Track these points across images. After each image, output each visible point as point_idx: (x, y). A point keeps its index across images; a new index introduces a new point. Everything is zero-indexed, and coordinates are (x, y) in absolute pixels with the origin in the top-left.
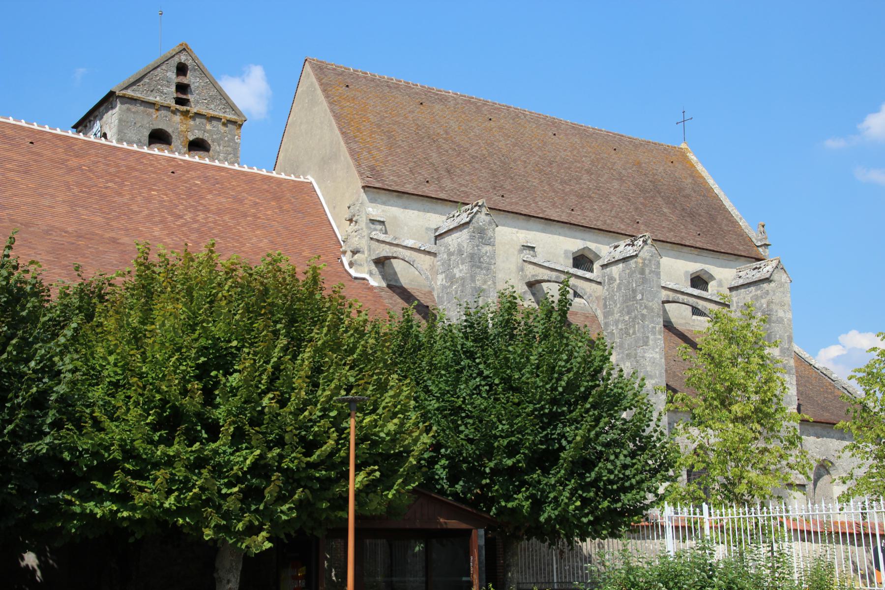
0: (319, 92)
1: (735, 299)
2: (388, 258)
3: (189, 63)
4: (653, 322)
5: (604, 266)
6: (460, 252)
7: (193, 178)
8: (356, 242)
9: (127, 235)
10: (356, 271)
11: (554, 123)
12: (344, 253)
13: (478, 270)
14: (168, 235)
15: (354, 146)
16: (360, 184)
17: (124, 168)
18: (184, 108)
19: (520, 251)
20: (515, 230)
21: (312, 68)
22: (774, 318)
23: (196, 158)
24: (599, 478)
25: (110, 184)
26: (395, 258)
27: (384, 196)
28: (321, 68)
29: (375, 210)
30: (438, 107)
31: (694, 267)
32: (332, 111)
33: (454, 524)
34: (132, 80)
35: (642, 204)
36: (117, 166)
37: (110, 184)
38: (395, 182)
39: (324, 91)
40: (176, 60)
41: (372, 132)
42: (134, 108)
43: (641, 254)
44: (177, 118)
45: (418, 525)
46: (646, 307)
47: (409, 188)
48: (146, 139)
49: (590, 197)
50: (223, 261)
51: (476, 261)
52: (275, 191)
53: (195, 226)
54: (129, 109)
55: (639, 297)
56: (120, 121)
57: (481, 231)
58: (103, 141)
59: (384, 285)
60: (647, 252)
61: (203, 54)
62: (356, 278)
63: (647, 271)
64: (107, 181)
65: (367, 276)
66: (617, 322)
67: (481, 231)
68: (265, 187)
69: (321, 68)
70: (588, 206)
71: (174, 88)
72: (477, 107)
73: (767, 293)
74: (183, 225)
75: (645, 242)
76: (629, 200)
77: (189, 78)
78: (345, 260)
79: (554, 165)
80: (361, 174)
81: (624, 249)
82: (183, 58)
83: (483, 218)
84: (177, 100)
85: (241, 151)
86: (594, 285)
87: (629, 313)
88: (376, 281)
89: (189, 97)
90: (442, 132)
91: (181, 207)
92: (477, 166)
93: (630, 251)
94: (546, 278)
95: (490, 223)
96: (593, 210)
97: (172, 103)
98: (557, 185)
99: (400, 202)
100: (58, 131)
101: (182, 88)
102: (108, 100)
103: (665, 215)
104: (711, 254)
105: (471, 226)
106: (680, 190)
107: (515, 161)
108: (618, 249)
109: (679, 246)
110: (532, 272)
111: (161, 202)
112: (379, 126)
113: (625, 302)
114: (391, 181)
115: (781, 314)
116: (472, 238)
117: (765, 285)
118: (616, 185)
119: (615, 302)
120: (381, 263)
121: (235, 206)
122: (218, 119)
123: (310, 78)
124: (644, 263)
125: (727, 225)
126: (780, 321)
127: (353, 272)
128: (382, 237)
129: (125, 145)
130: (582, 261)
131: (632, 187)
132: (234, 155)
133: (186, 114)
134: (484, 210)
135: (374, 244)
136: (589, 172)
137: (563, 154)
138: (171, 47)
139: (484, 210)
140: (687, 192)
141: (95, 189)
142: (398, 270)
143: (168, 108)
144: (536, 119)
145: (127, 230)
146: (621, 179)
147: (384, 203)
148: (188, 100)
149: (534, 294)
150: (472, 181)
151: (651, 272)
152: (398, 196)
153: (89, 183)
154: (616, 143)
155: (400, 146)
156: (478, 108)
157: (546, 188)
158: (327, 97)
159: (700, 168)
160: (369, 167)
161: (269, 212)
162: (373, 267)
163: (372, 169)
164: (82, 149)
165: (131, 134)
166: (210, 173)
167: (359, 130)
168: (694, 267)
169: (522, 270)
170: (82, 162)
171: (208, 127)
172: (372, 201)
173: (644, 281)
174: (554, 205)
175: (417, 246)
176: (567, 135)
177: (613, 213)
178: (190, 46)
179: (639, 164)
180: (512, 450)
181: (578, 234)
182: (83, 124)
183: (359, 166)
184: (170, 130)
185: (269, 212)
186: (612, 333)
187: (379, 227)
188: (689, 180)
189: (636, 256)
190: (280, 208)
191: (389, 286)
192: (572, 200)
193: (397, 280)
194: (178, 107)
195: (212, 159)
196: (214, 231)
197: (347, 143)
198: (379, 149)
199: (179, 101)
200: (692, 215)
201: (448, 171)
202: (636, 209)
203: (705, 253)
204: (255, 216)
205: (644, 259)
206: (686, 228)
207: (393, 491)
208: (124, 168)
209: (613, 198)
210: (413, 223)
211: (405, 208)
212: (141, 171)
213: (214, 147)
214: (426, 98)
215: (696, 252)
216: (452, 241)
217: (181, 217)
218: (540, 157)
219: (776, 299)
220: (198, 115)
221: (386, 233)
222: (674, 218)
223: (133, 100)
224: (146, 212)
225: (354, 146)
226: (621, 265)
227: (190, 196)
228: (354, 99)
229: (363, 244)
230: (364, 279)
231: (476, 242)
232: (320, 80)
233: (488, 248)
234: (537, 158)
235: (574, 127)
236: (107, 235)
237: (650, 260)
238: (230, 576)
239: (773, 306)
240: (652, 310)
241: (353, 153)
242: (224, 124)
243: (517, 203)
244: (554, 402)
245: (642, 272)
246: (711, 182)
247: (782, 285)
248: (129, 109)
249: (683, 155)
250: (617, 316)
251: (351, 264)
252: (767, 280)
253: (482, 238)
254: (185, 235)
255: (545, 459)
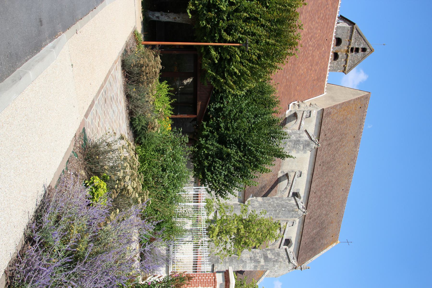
0: (358, 96)
1: (282, 250)
2: (288, 178)
3: (367, 53)
4: (274, 214)
5: (286, 249)
6: (300, 137)
7: (325, 47)
8: (302, 105)
9: (304, 18)
10: (292, 106)
11: (347, 190)
12: (298, 102)
13: (293, 143)
14: (304, 34)
15: (338, 107)
16: (324, 108)
17: (328, 21)
18: (350, 51)
19: (299, 171)
20: (307, 169)
21: (367, 95)
22: (275, 263)
23: (331, 57)
24: (215, 162)
25: (322, 15)
26: (288, 180)
27: (320, 117)
28: (367, 98)
29: (314, 114)
30: (353, 143)
31: (293, 240)
32: (351, 100)
33: (199, 108)
34: (359, 31)
35: (317, 222)
36: (329, 19)
37: (322, 15)
38: (325, 122)
39: (359, 98)
40: (368, 48)
41: (344, 115)
42: (349, 32)
43: (299, 210)
44: (346, 48)
45: (198, 93)
46: (279, 212)
47: (323, 127)
48: (338, 36)
49: (320, 201)
50: (298, 31)
51: (297, 142)
52: (321, 79)
53: (307, 45)
54: (348, 30)
55: (283, 209)
56: (344, 27)
57: (308, 145)
58: (336, 23)
59: (287, 116)
60: (300, 213)
61: (370, 58)
62: (289, 106)
63: (293, 213)
64: (323, 14)
65: (290, 109)
66: (273, 202)
67: (308, 145)
68: (322, 75)
69: (367, 98)
70: (316, 200)
71: (357, 47)
72: (353, 159)
73: (285, 261)
74: (308, 41)
75: (304, 212)
76: (318, 217)
77: (361, 53)
78: (296, 102)
79: (332, 188)
80: (328, 108)
81: (301, 205)
82: (368, 50)
83: (313, 145)
84: (352, 49)
85: (334, 73)
86: (287, 195)
87: (277, 206)
88: (288, 113)
89: (354, 53)
90: (344, 144)
91: (314, 41)
92: (331, 156)
93: (301, 207)
94: (290, 179)
95: (312, 148)
96: (315, 201)
97: (351, 46)
98: (324, 188)
99: (318, 123)
100: (338, 10)
101: (357, 50)
102: (352, 23)
103: (313, 230)
104: (298, 247)
105: (310, 141)
106: (322, 238)
107: (333, 172)
108: (301, 203)
109: (301, 234)
110: (291, 176)
111: (316, 34)
112: (346, 118)
113: (281, 204)
114: (326, 120)
115: (277, 266)
116: (306, 141)
117: (287, 260)
118: (324, 212)
119: (281, 201)
120: (295, 115)
121: (315, 62)
122: (346, 64)
123: (363, 94)
124: (296, 211)
125: (309, 255)
126: (274, 265)
127: (291, 105)
128: (305, 115)
129: (335, 30)
130: (288, 242)
131: (323, 219)
132: (333, 70)
133: (348, 51)
134: (316, 146)
135: (302, 112)
136: (329, 202)
137: (336, 192)
138: (372, 47)
139: (316, 146)
140: (321, 241)
141: (320, 9)
142: (292, 122)
143: (350, 44)
144: (349, 183)
145: (306, 19)
146: (326, 215)
147: (317, 117)
148: (352, 52)
149: (283, 176)
150: (326, 153)
151: (293, 214)
152: (309, 180)
153: (322, 7)
154: (340, 215)
155: (338, 126)
156: (352, 160)
157: (323, 184)
158: (356, 99)
159: (330, 247)
160: (331, 112)
161: (313, 75)
162: (293, 112)
163: (330, 113)
164: (334, 6)
165: (339, 31)
166: (327, 54)
167: (344, 110)
168: (293, 240)
169: (292, 172)
170: (330, 5)
171: (343, 60)
172: (318, 112)
173: (289, 211)
174: (317, 186)
175: (302, 125)
176: (343, 195)
177: (314, 210)
178: (373, 53)
179: (332, 223)
180: (227, 128)
181: (306, 194)
182: (342, 18)
183: (331, 108)
184: (341, 45)
185: (313, 75)
186: (269, 200)
187: (308, 115)
188: (326, 242)
189: (299, 209)
190: (314, 80)
191: (286, 118)
192: (319, 194)
193: (288, 122)
194: (350, 48)
195: (333, 48)
196: (306, 53)
197: (339, 104)
198: (337, 117)
199: (352, 49)
200: (313, 242)
201: (329, 144)
202: (315, 219)
203: (299, 245)
204: (311, 69)
205: (297, 212)
206: (308, 238)
207: (210, 72)
208: (328, 21)
209: (319, 210)
210: (311, 126)
211: (315, 126)
212: (327, 28)
213: (335, 62)
214: (356, 139)
215: (299, 241)
216: (305, 135)
217: (310, 40)
218: (335, 183)
219: (282, 264)
220: (347, 56)
221: (306, 118)
222: (312, 234)
223: (352, 32)
224: (312, 27)
225: (338, 107)
226: (295, 203)
227: (318, 45)
228: (356, 110)
229: (302, 109)
230: (289, 109)
231: (304, 143)
232: (363, 97)
233: (302, 147)
234: (334, 181)
235: (346, 198)
236: (304, 11)
237: (297, 214)
238: (181, 18)
239: (279, 263)
240: (278, 214)
241: (335, 106)
242: (344, 66)
243: (317, 170)
244: (245, 145)
245: (293, 211)
246: (325, 251)
247: (287, 267)
248: (348, 30)
249: (335, 241)
250: (276, 202)
251: (294, 104)
252: (289, 261)
253: (306, 145)
254: (304, 41)
255: (222, 140)
